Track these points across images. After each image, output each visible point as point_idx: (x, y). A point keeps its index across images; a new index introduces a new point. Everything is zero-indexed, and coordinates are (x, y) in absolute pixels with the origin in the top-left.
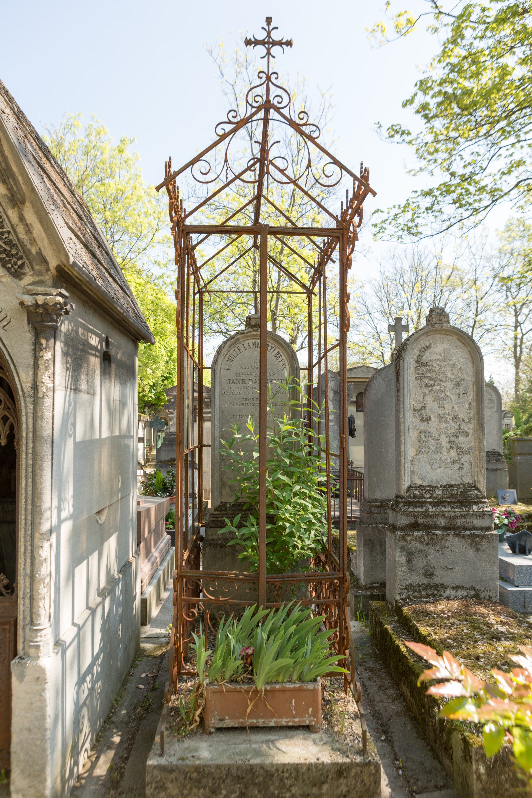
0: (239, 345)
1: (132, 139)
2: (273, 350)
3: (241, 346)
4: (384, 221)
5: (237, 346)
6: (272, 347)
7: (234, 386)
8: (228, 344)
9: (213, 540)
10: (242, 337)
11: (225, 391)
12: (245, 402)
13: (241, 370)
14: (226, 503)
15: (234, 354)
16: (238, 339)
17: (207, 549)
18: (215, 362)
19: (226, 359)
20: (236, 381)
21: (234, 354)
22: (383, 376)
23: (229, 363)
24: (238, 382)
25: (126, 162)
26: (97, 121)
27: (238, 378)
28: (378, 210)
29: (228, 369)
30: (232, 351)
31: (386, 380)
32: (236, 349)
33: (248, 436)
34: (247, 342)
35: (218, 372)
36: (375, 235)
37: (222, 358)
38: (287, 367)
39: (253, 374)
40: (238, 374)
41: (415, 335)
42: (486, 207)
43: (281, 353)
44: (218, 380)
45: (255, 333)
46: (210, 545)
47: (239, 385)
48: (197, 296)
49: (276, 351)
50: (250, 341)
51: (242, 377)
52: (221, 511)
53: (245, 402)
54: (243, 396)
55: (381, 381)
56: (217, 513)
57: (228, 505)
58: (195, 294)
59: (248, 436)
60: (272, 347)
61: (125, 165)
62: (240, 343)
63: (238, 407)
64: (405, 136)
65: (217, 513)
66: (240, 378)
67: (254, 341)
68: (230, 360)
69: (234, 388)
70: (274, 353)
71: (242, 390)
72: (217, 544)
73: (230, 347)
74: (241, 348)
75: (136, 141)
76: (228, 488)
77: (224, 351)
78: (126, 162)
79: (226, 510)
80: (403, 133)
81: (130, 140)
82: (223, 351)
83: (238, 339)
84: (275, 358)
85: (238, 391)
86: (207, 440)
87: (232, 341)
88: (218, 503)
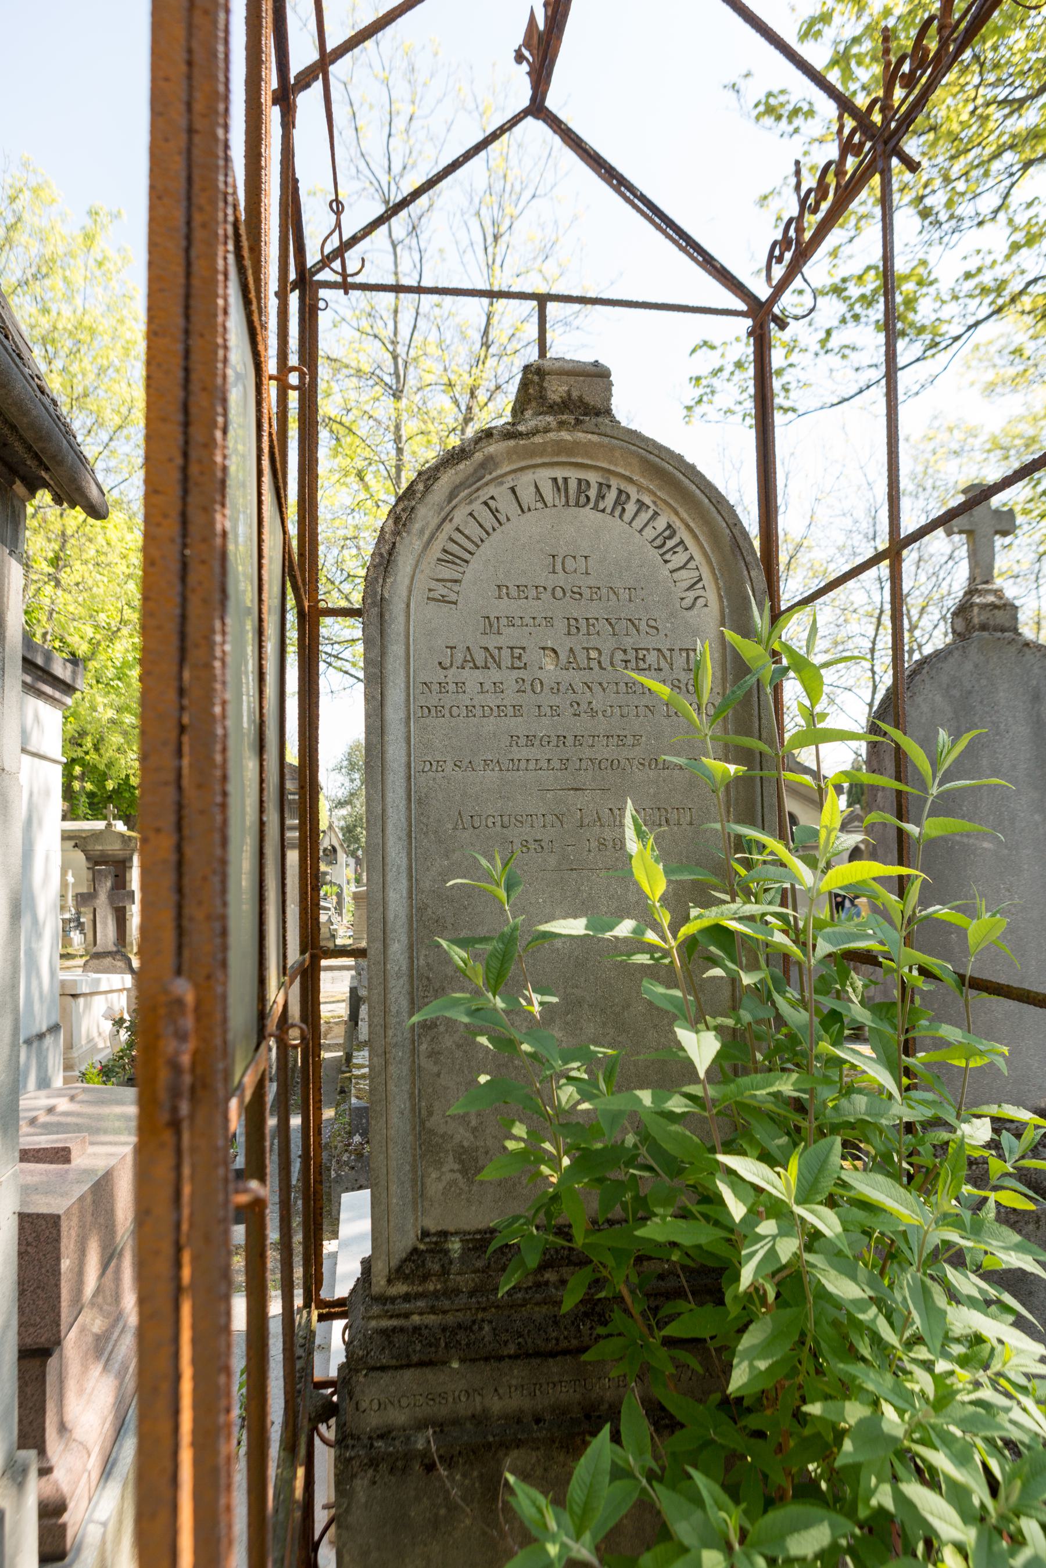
0: (492, 490)
1: (115, 211)
2: (644, 516)
3: (501, 493)
4: (717, 372)
5: (484, 494)
6: (641, 505)
7: (472, 678)
8: (447, 479)
9: (385, 1434)
10: (510, 454)
11: (433, 701)
12: (525, 753)
13: (504, 607)
14: (444, 1234)
15: (473, 530)
16: (488, 464)
17: (360, 1485)
18: (383, 562)
19: (435, 551)
20: (480, 657)
21: (473, 530)
22: (945, 679)
23: (446, 572)
24: (492, 659)
25: (100, 264)
26: (35, 172)
27: (492, 642)
28: (705, 343)
29: (443, 600)
30: (460, 516)
31: (956, 693)
32: (477, 507)
33: (625, 928)
34: (528, 477)
35: (397, 609)
36: (689, 408)
37: (418, 544)
38: (711, 596)
39: (561, 625)
40: (490, 625)
41: (218, 852)
42: (956, 339)
43: (683, 534)
44: (396, 649)
45: (565, 435)
46: (373, 1463)
47: (494, 674)
48: (294, 298)
49: (661, 523)
50: (544, 475)
51: (509, 636)
52: (425, 1278)
53: (525, 753)
54: (518, 726)
55: (938, 698)
56: (401, 1288)
57: (455, 1246)
58: (282, 296)
59: (625, 928)
60: (641, 505)
61: (98, 273)
62: (498, 480)
63: (492, 776)
64: (799, 121)
65: (401, 1288)
66: (501, 641)
67: (559, 473)
68: (449, 558)
69: (472, 686)
70: (649, 533)
71: (510, 697)
72: (408, 1457)
73: (452, 496)
74: (505, 504)
75: (123, 211)
76: (450, 1163)
77: (426, 515)
78: (100, 264)
79: (445, 1272)
80: (796, 112)
81: (110, 214)
82: (422, 511)
83: (488, 464)
84: (655, 554)
85: (492, 700)
86: (341, 925)
87: (465, 467)
88: (405, 1242)
